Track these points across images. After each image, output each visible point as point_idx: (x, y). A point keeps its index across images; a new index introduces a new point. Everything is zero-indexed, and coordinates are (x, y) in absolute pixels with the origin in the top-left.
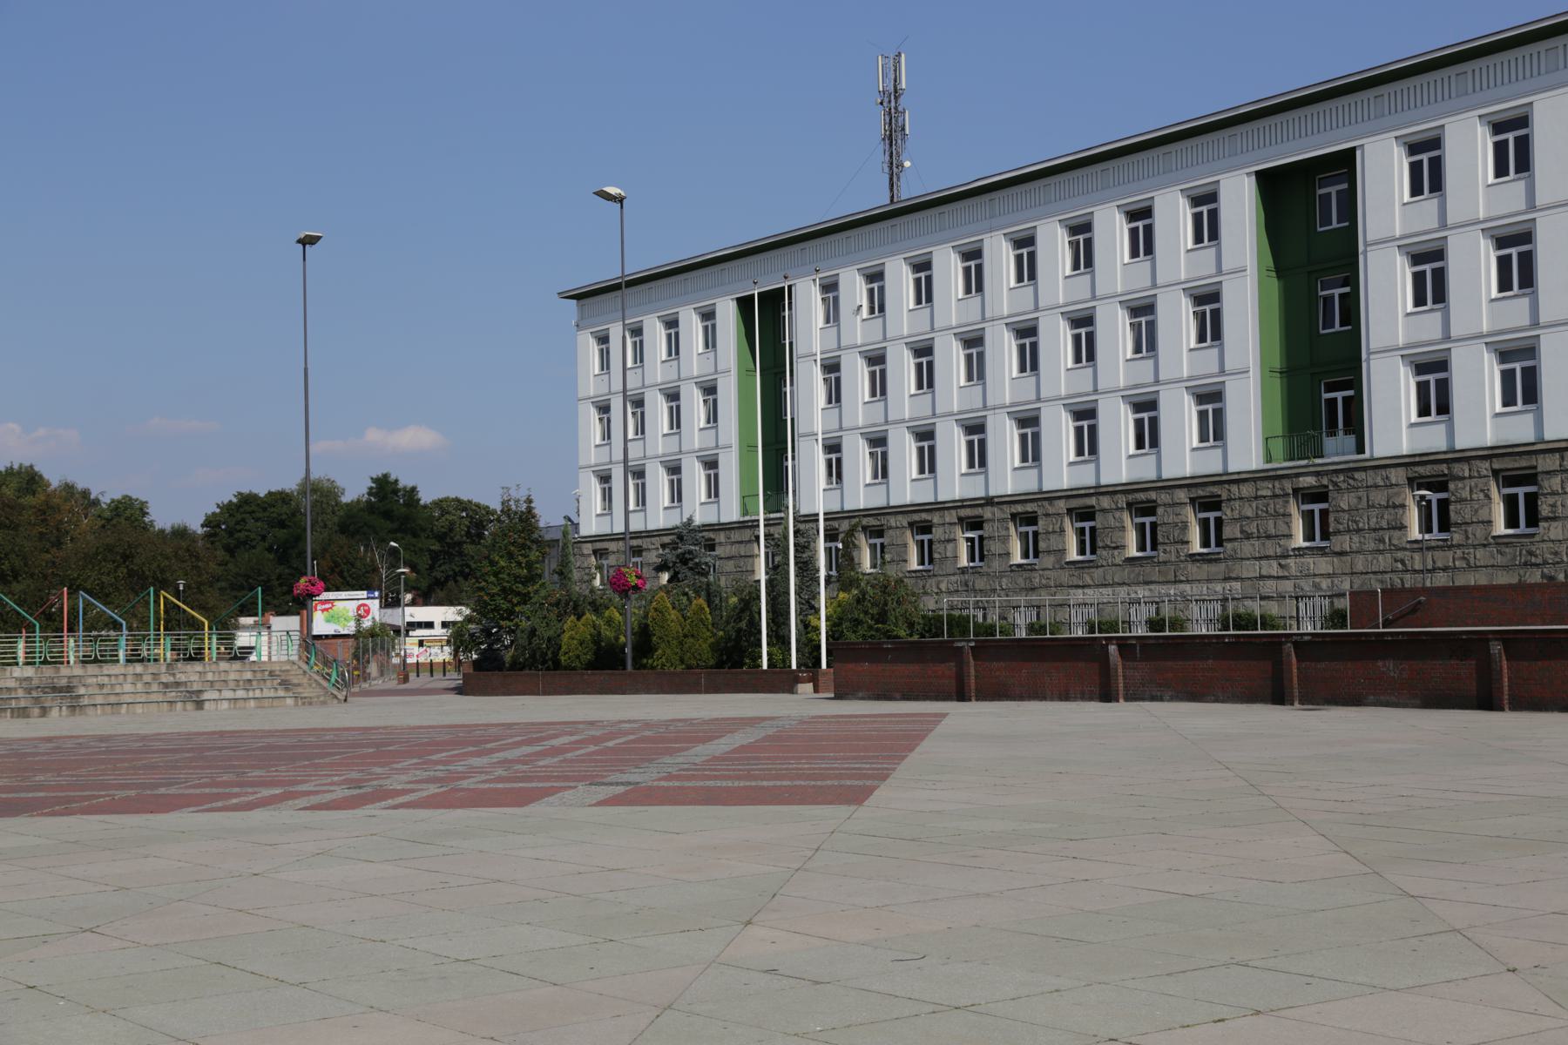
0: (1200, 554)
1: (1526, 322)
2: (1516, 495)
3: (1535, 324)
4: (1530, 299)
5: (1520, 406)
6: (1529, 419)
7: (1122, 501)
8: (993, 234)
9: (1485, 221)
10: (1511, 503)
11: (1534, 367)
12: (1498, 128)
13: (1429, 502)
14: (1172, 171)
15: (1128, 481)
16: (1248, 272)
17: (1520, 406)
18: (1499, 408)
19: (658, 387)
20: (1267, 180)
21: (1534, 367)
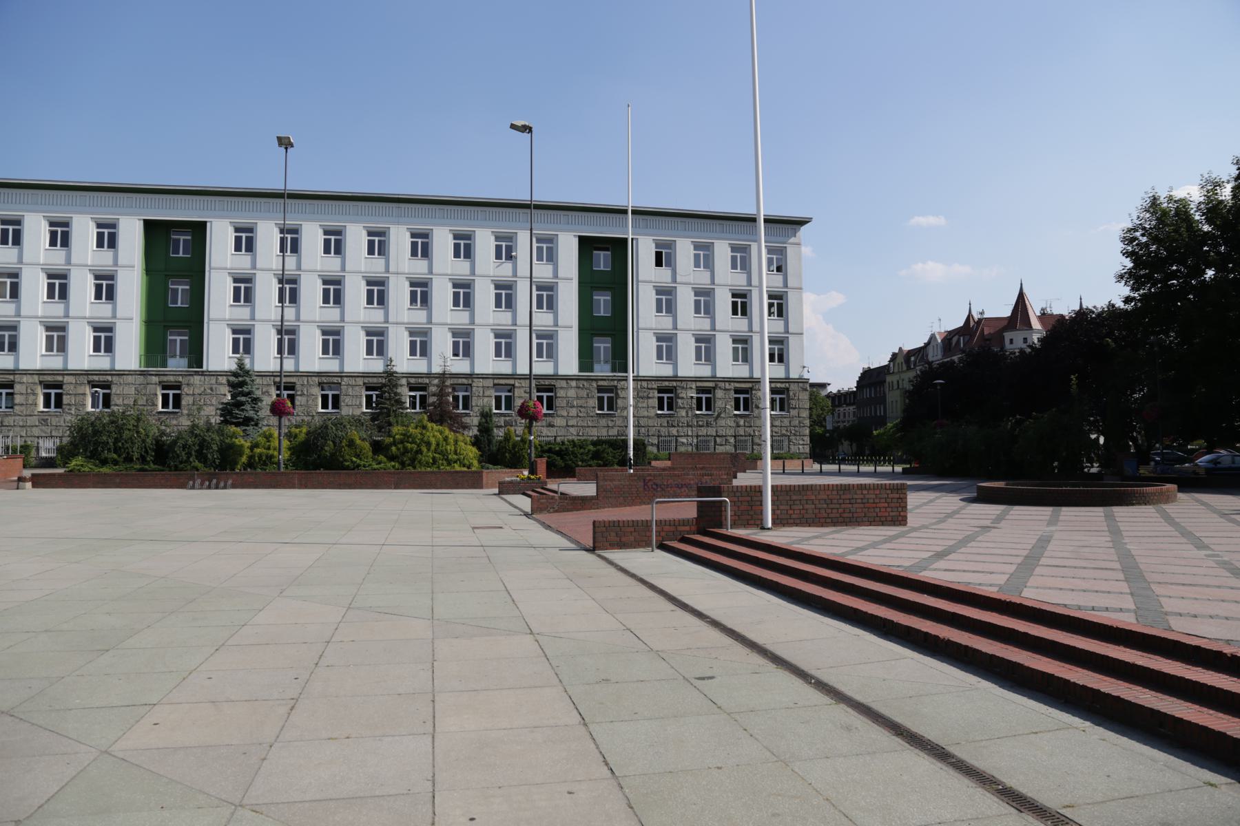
0: (43, 412)
1: (13, 313)
2: (168, 394)
3: (67, 316)
4: (427, 312)
5: (102, 353)
6: (61, 359)
7: (360, 381)
8: (399, 226)
9: (42, 265)
10: (47, 397)
11: (64, 336)
12: (456, 237)
13: (99, 394)
14: (132, 207)
15: (40, 369)
16: (136, 268)
17: (102, 353)
18: (44, 352)
19: (89, 268)
20: (150, 226)
21: (64, 336)
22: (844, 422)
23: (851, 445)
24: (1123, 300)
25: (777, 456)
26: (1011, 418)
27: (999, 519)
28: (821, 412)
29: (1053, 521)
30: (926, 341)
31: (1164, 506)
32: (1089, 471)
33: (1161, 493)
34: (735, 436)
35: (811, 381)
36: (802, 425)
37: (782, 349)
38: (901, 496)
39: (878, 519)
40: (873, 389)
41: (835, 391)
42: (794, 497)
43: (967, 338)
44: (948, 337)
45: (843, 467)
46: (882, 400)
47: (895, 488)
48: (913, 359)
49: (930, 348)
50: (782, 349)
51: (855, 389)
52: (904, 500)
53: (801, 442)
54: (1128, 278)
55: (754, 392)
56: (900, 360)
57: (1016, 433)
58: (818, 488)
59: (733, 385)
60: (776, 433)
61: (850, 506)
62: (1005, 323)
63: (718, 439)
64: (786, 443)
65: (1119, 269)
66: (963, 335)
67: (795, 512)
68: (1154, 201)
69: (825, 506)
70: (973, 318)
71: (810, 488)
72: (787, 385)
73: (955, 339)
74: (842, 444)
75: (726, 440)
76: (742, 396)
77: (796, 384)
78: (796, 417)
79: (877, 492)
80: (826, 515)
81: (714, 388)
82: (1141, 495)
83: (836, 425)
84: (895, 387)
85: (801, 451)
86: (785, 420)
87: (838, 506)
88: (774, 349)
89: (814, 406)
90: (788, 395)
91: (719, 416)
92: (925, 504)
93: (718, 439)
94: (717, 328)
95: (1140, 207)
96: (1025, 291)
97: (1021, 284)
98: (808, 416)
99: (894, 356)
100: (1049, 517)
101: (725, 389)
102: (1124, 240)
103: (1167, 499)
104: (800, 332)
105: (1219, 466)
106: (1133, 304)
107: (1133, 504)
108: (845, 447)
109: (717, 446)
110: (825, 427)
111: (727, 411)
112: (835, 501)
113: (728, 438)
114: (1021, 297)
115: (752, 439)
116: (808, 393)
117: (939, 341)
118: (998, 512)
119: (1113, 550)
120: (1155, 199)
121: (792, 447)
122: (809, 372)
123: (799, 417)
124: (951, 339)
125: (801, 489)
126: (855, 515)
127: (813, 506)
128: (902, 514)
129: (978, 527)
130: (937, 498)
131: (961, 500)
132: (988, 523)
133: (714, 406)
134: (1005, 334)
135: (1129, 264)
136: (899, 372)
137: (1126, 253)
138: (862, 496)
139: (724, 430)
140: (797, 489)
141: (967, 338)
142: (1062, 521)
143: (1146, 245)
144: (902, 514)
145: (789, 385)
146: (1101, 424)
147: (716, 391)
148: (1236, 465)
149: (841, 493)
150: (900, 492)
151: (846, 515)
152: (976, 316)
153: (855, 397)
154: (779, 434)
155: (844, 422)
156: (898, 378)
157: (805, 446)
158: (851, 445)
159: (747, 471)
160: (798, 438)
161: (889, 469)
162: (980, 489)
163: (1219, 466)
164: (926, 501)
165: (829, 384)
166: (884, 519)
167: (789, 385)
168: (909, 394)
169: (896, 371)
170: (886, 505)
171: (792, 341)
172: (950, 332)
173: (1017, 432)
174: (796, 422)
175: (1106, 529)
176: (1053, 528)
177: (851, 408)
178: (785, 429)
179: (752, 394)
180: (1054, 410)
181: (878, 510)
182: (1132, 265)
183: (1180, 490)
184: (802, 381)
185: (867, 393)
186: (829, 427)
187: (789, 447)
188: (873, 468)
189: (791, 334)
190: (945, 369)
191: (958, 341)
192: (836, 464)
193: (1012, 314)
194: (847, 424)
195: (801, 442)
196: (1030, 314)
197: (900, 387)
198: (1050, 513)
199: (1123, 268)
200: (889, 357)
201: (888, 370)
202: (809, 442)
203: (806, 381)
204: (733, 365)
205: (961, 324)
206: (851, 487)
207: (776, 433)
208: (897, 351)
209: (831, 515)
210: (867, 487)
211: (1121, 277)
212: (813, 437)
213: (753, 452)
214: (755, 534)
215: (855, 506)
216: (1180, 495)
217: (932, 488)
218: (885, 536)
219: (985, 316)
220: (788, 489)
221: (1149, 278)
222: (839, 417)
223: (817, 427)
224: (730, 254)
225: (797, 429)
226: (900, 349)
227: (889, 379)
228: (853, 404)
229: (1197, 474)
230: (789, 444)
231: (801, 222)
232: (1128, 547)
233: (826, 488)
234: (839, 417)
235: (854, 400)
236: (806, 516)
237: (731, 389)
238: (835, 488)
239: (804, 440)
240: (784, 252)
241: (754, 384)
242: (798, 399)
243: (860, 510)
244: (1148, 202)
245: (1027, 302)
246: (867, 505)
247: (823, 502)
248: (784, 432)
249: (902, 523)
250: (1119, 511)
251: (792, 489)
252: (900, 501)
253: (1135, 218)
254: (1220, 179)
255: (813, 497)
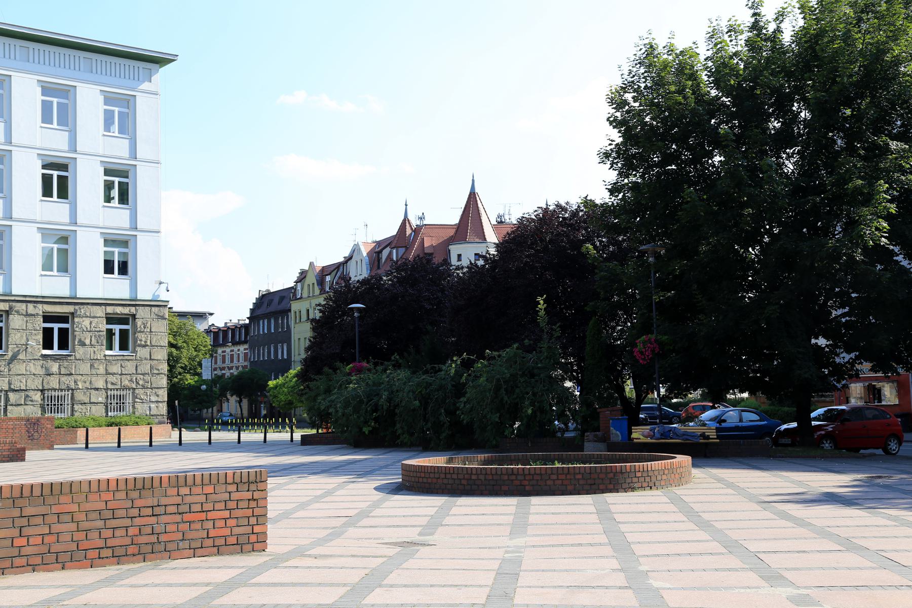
22: (231, 368)
23: (240, 402)
24: (610, 187)
25: (113, 420)
26: (455, 359)
27: (433, 525)
28: (195, 353)
29: (519, 527)
30: (347, 255)
31: (679, 491)
32: (562, 435)
33: (672, 470)
34: (42, 391)
35: (177, 308)
36: (156, 372)
37: (126, 254)
38: (257, 495)
39: (209, 542)
40: (273, 321)
41: (221, 325)
42: (29, 511)
43: (402, 251)
44: (377, 250)
45: (216, 435)
46: (285, 337)
47: (245, 479)
48: (328, 278)
49: (352, 265)
50: (126, 254)
51: (247, 321)
52: (261, 503)
53: (154, 398)
54: (615, 158)
55: (76, 320)
56: (311, 279)
57: (463, 379)
58: (85, 488)
59: (41, 309)
60: (112, 384)
61: (154, 519)
62: (452, 232)
63: (11, 395)
64: (129, 400)
65: (604, 145)
66: (397, 247)
67: (32, 541)
68: (651, 49)
69: (100, 524)
70: (409, 223)
71: (66, 489)
72: (133, 310)
73: (385, 253)
74: (228, 400)
75: (27, 396)
76: (56, 326)
77: (148, 308)
78: (146, 359)
79: (209, 489)
80: (101, 543)
81: (8, 313)
82: (645, 474)
83: (219, 373)
84: (304, 318)
85: (154, 412)
86: (127, 363)
87: (128, 522)
88: (113, 253)
89: (185, 345)
90: (135, 326)
91: (14, 357)
92: (317, 499)
93: (11, 395)
94: (14, 215)
95: (633, 58)
96: (477, 190)
97: (473, 181)
98: (166, 358)
99: (303, 275)
100: (512, 517)
101: (27, 315)
102: (612, 101)
103: (681, 479)
104: (155, 228)
105: (724, 425)
106: (620, 196)
107: (633, 489)
108: (232, 405)
109: (9, 408)
110: (200, 375)
111: (29, 350)
112: (122, 513)
113: (31, 393)
114: (473, 197)
115: (72, 394)
116: (166, 322)
117: (365, 254)
118: (432, 511)
119: (630, 592)
120: (651, 47)
121: (138, 406)
122: (168, 291)
123: (151, 359)
124: (381, 252)
125: (47, 491)
126: (163, 538)
127: (73, 526)
128: (257, 529)
129: (396, 544)
130: (340, 486)
131: (376, 489)
132: (412, 534)
133: (7, 341)
134: (450, 247)
135: (616, 136)
136: (309, 297)
137: (615, 120)
138: (178, 500)
139: (24, 381)
140: (37, 492)
141: (402, 251)
142: (532, 524)
143: (639, 114)
144: (257, 529)
145: (136, 310)
146: (575, 368)
147: (11, 317)
148: (744, 424)
149: (135, 494)
150: (253, 487)
151: (143, 539)
152: (415, 222)
153: (247, 334)
154: (119, 387)
155: (231, 368)
156: (308, 306)
157: (160, 405)
158: (240, 402)
159: (55, 447)
160: (149, 391)
161: (285, 436)
162: (408, 471)
163: (724, 425)
164: (319, 493)
165: (211, 314)
166: (222, 542)
167: (136, 310)
168: (317, 325)
169: (305, 295)
170: (226, 514)
171: (143, 242)
172: (378, 243)
173: (464, 378)
174: (145, 367)
175: (603, 539)
176: (519, 541)
177: (242, 348)
178: (129, 377)
179: (73, 323)
180: (515, 346)
181: (209, 525)
182: (621, 139)
183: (694, 465)
184: (157, 305)
185: (263, 327)
186: (207, 375)
187: (134, 407)
188: (235, 435)
189: (140, 231)
190: (370, 286)
191: (390, 253)
192: (206, 430)
193: (460, 221)
194: (235, 372)
195: (154, 398)
196: (483, 221)
197: (311, 317)
198: (513, 509)
199: (610, 142)
200: (295, 276)
201: (295, 294)
202: (166, 399)
203: (163, 305)
204: (42, 275)
205: (392, 231)
206: (156, 483)
207: (112, 384)
208: (307, 268)
209: (110, 543)
210: (190, 481)
211: (607, 155)
212: (174, 392)
213: (72, 415)
214: (333, 458)
215: (164, 519)
216: (696, 472)
217: (335, 468)
218: (208, 584)
219: (425, 223)
220: (16, 493)
221: (643, 159)
222: (224, 362)
223: (188, 376)
224: (39, 98)
225: (147, 378)
226: (311, 264)
227: (295, 306)
228: (245, 342)
229: (708, 438)
230: (134, 402)
231: (159, 61)
232: (656, 584)
233: (103, 486)
234: (224, 362)
235: (246, 337)
236: (56, 548)
237: (37, 314)
238: (122, 486)
239: (158, 396)
240: (131, 103)
241: (77, 307)
242: (151, 332)
243: (174, 528)
244: (643, 51)
245: (480, 205)
246: (187, 517)
247: (95, 515)
248: (126, 383)
249: (257, 546)
250: (611, 498)
251: (26, 493)
252: (253, 504)
253: (626, 73)
254: (736, 20)
255: (75, 508)
